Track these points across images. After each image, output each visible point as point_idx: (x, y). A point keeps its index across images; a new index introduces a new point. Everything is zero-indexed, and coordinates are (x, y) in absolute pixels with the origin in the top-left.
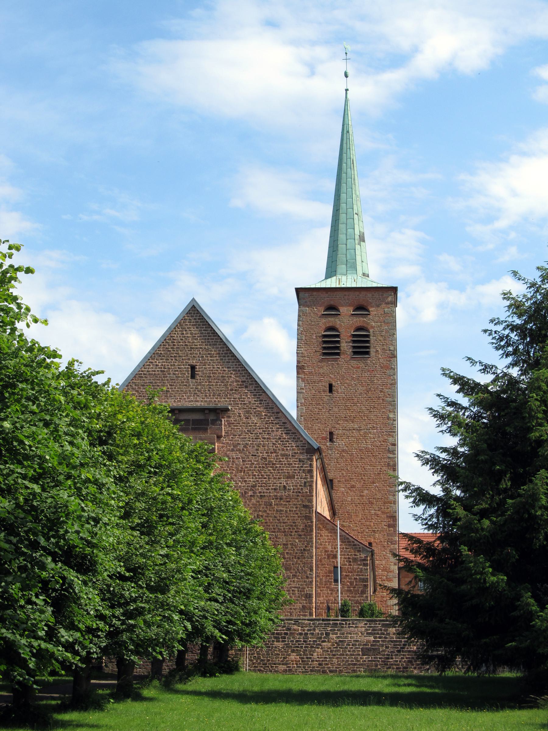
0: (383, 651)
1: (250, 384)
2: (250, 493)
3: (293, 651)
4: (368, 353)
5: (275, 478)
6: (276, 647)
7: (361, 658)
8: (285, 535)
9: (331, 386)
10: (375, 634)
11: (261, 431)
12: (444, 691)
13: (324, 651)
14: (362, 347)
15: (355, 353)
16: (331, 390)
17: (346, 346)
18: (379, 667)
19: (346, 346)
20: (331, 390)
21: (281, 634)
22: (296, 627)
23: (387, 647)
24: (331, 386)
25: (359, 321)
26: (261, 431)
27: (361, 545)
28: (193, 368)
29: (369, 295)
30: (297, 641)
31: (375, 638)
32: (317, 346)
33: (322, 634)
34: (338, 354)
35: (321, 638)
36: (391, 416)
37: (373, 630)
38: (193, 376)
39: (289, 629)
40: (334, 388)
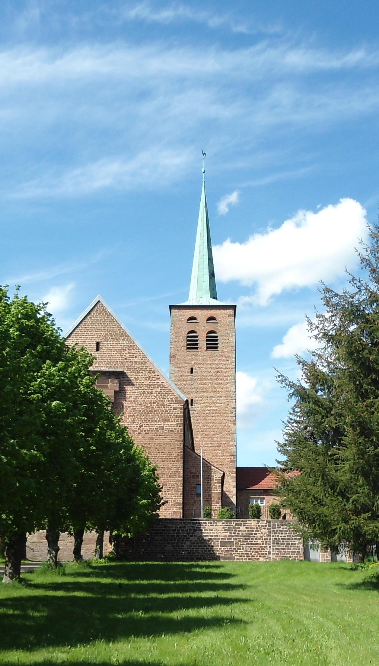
0: (236, 543)
1: (139, 356)
2: (139, 431)
3: (168, 543)
4: (217, 348)
5: (156, 421)
6: (156, 540)
7: (220, 549)
8: (162, 461)
9: (192, 369)
10: (230, 530)
11: (146, 388)
12: (111, 616)
13: (192, 543)
14: (212, 343)
15: (208, 348)
16: (192, 372)
17: (202, 343)
18: (233, 555)
19: (202, 343)
20: (192, 372)
21: (160, 530)
22: (170, 525)
23: (240, 541)
24: (192, 369)
25: (210, 327)
26: (146, 388)
27: (216, 469)
28: (98, 344)
29: (218, 311)
30: (171, 536)
31: (231, 533)
32: (183, 343)
33: (190, 530)
34: (197, 348)
35: (190, 533)
36: (233, 389)
37: (229, 528)
38: (98, 350)
39: (166, 527)
40: (194, 371)
